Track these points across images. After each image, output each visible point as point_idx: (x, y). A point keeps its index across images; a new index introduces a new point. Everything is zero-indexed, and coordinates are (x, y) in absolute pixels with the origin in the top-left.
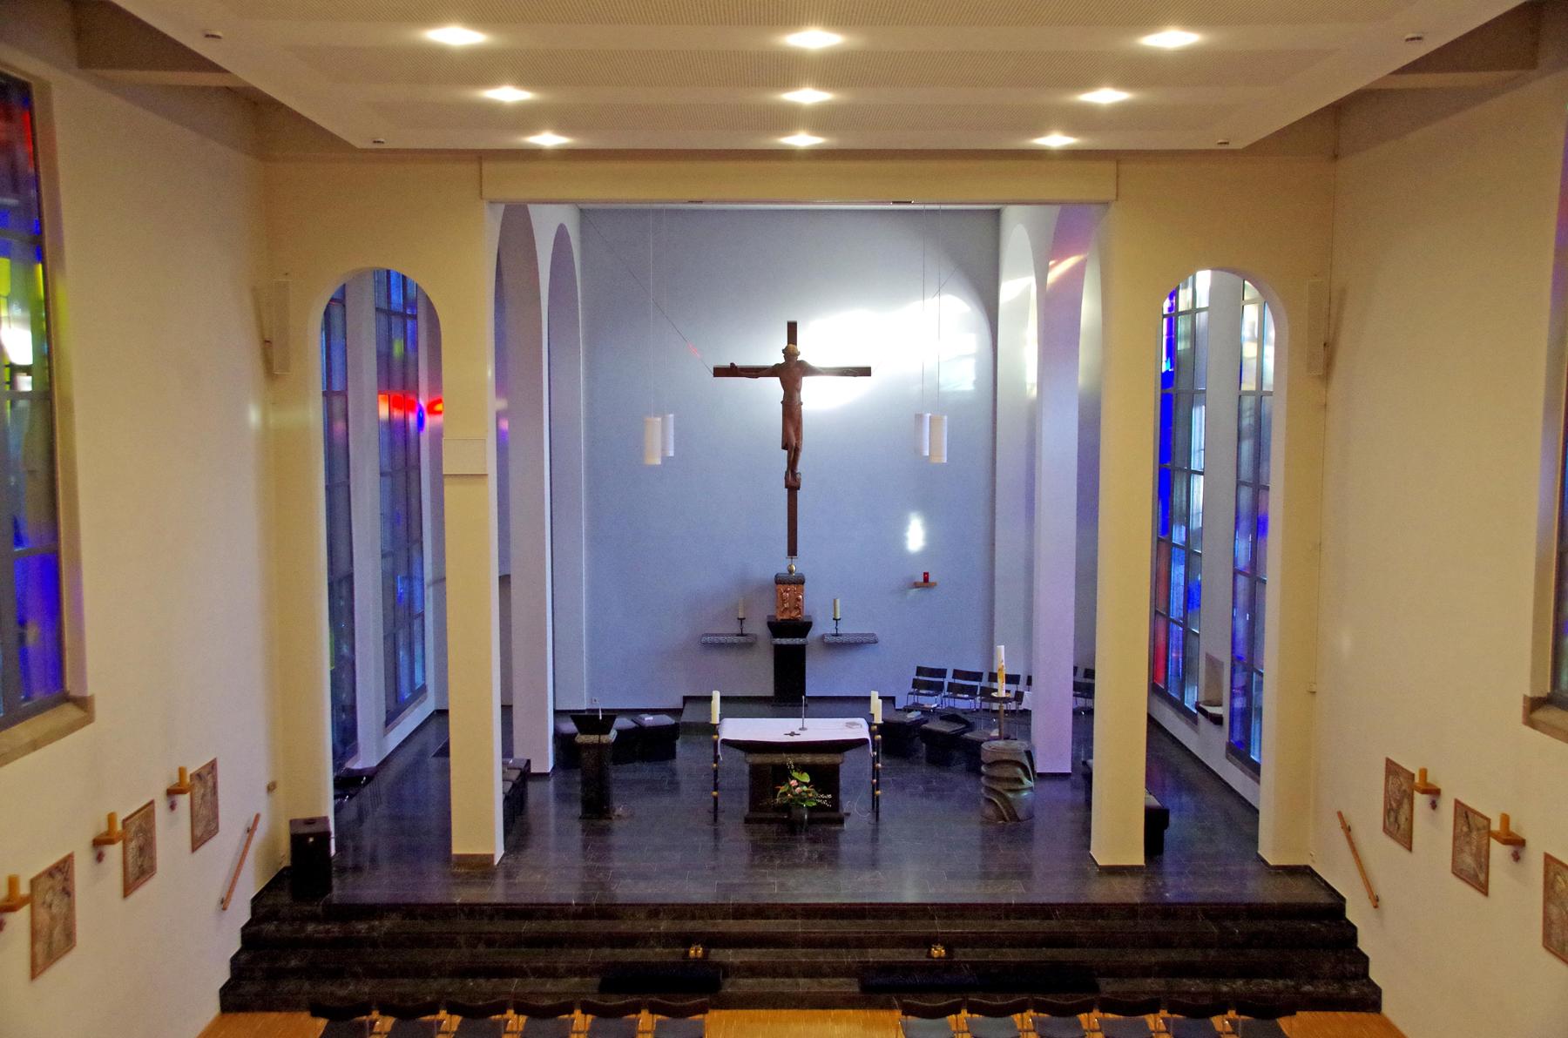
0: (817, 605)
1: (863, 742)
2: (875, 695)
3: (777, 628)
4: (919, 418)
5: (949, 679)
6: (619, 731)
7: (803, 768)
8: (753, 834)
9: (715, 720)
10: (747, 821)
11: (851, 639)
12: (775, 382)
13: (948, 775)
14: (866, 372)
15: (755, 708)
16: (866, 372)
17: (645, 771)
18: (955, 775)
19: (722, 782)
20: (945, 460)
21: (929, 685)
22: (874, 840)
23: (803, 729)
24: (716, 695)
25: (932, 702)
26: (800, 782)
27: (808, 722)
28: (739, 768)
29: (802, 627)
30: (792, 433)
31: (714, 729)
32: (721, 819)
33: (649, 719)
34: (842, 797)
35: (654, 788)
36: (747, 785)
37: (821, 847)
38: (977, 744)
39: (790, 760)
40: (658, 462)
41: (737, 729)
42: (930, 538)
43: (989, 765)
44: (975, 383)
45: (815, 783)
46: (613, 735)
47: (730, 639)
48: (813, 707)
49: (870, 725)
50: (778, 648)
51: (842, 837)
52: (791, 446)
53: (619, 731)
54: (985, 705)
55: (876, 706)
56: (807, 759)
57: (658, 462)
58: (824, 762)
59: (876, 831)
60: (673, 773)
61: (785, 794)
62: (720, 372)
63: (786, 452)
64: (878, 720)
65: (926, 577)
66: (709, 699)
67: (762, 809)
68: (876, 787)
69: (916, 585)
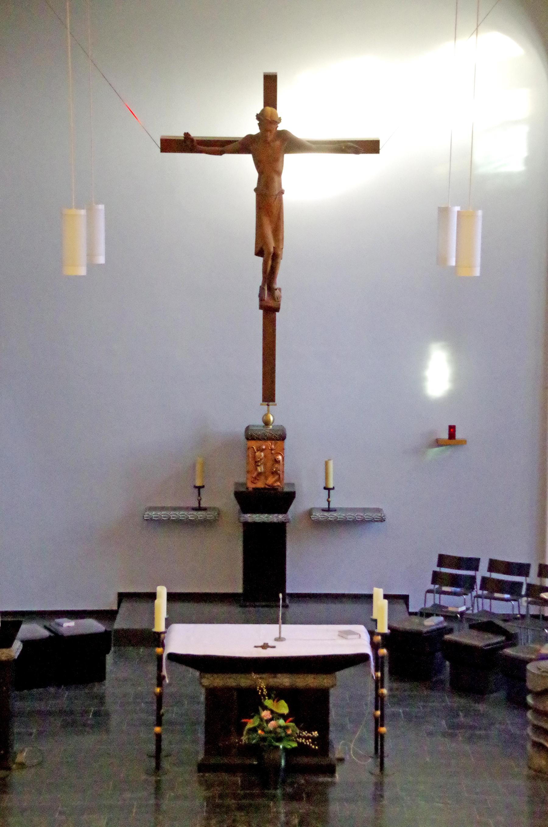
0: (302, 470)
1: (361, 659)
2: (378, 593)
3: (248, 500)
4: (444, 212)
5: (483, 571)
6: (26, 643)
7: (278, 693)
8: (209, 786)
9: (160, 626)
10: (202, 768)
11: (350, 516)
12: (246, 161)
13: (481, 707)
14: (372, 147)
15: (207, 608)
16: (372, 147)
17: (64, 698)
18: (494, 711)
19: (170, 713)
20: (477, 272)
21: (454, 581)
22: (378, 796)
23: (279, 639)
24: (162, 592)
25: (459, 604)
26: (274, 716)
27: (288, 629)
28: (190, 692)
29: (282, 500)
30: (269, 231)
31: (157, 640)
32: (166, 764)
33: (68, 626)
34: (332, 736)
35: (72, 722)
36: (203, 718)
37: (303, 807)
38: (520, 665)
39: (262, 682)
40: (82, 271)
41: (190, 638)
42: (458, 378)
43: (538, 695)
44: (528, 161)
45: (294, 715)
46: (17, 647)
47: (181, 515)
48: (295, 608)
49: (372, 633)
50: (247, 525)
51: (334, 793)
52: (268, 252)
53: (26, 643)
54: (534, 610)
55: (381, 608)
56: (284, 680)
57: (82, 271)
58: (306, 687)
59: (379, 786)
60: (101, 699)
61: (254, 730)
62: (169, 145)
63: (261, 260)
64: (383, 628)
65: (452, 430)
66: (152, 596)
67: (225, 751)
68: (379, 722)
69: (438, 443)
